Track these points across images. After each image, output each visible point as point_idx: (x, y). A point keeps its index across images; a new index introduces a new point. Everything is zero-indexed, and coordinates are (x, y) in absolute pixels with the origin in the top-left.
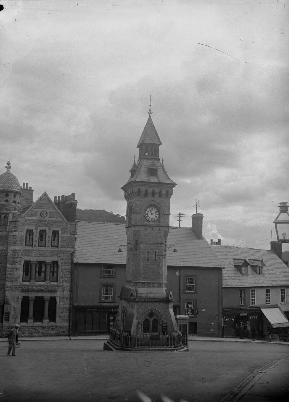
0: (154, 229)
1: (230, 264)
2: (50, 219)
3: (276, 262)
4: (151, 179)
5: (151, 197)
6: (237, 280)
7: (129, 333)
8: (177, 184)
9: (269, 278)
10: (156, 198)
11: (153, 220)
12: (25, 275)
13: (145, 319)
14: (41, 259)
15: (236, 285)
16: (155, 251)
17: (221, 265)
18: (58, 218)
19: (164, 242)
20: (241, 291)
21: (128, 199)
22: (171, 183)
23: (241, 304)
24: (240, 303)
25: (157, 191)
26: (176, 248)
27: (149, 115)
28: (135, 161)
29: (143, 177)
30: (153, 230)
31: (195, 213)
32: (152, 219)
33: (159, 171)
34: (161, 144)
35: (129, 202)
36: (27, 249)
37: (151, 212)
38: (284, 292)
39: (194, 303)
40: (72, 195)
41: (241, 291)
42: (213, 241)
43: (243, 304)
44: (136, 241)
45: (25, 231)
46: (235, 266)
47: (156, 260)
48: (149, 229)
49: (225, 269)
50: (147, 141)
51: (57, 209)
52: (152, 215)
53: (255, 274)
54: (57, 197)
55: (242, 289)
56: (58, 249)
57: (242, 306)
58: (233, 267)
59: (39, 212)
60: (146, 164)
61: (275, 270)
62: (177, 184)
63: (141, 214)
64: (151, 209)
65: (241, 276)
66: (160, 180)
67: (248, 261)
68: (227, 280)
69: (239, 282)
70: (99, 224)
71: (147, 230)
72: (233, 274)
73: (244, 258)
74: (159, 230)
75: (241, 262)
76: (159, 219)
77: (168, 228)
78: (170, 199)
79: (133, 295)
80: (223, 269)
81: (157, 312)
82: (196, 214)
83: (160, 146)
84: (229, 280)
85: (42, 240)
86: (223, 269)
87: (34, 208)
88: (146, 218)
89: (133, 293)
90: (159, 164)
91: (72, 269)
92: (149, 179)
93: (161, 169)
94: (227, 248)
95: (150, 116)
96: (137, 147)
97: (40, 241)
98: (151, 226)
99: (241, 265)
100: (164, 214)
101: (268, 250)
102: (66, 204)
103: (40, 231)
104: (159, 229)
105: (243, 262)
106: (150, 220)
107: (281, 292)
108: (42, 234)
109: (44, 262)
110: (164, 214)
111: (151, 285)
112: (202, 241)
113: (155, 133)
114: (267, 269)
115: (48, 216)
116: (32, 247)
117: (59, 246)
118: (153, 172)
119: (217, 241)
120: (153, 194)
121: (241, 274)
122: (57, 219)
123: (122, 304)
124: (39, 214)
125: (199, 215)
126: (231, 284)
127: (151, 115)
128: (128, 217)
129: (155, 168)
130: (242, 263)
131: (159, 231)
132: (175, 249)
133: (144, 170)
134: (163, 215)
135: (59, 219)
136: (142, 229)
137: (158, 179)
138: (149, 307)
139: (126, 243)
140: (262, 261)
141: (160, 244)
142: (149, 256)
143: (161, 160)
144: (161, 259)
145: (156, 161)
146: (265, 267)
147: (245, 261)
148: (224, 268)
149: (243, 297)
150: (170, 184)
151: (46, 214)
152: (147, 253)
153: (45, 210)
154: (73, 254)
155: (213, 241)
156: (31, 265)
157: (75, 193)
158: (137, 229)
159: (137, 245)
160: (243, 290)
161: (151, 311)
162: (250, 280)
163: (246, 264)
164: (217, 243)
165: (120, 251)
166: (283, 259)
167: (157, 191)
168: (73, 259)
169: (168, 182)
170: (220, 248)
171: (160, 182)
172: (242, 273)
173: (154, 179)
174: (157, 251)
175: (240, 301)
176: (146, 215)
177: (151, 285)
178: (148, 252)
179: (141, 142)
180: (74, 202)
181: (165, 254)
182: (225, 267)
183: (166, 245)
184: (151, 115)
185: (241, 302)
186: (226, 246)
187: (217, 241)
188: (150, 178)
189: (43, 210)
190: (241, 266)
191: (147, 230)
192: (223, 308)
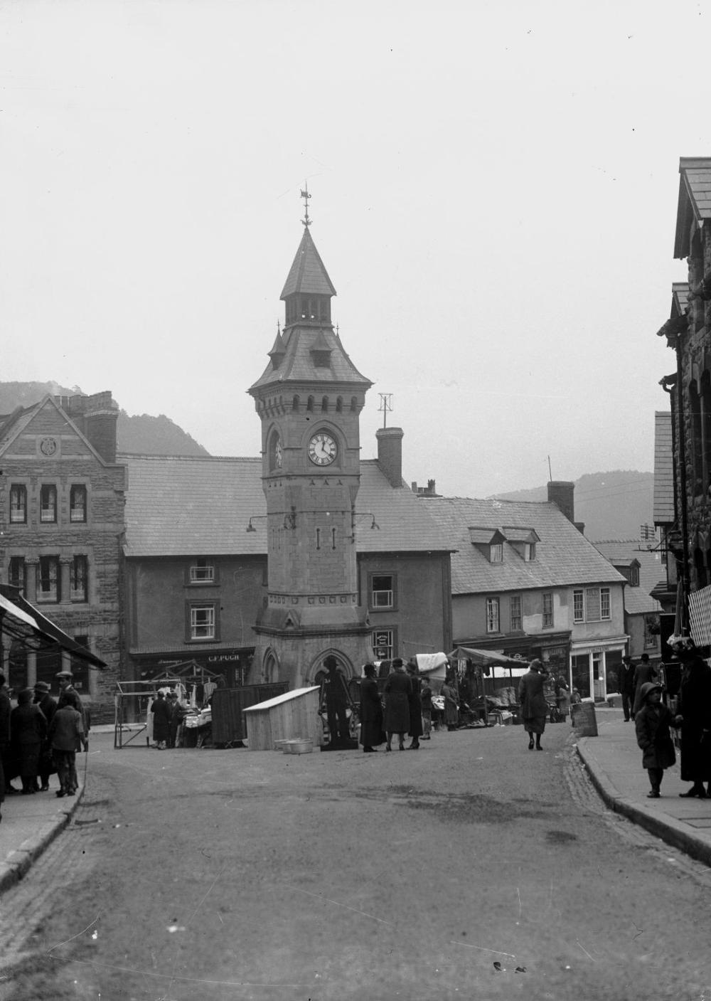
0: (329, 482)
1: (464, 541)
2: (65, 458)
3: (561, 529)
4: (318, 374)
5: (319, 412)
6: (480, 577)
7: (93, 716)
8: (373, 384)
9: (549, 567)
10: (332, 415)
11: (326, 461)
12: (198, 611)
13: (319, 670)
14: (48, 551)
15: (480, 589)
16: (332, 528)
17: (447, 545)
18: (81, 455)
19: (350, 509)
20: (490, 602)
21: (265, 416)
22: (362, 380)
23: (492, 629)
24: (489, 626)
25: (333, 399)
26: (375, 521)
27: (304, 227)
28: (279, 331)
29: (303, 370)
30: (328, 484)
31: (383, 427)
32: (322, 459)
33: (333, 354)
34: (335, 293)
35: (270, 423)
36: (14, 529)
37: (324, 444)
38: (581, 596)
39: (390, 633)
40: (103, 396)
41: (490, 602)
42: (418, 486)
43: (494, 630)
44: (293, 508)
45: (8, 487)
46: (474, 544)
47: (334, 548)
48: (319, 483)
49: (457, 553)
50: (305, 289)
51: (79, 432)
52: (321, 450)
53: (518, 560)
54: (61, 398)
55: (491, 596)
56: (87, 526)
57: (494, 633)
58: (471, 546)
59: (38, 443)
60: (305, 340)
61: (560, 548)
62: (373, 384)
63: (301, 451)
64: (325, 438)
65: (488, 566)
66: (338, 375)
67: (501, 531)
68: (460, 579)
69: (485, 580)
70: (166, 462)
71: (314, 484)
72: (471, 562)
73: (492, 526)
74: (338, 484)
75: (487, 534)
76: (336, 459)
77: (356, 477)
78: (360, 416)
79: (293, 621)
80: (451, 554)
81: (341, 655)
82: (385, 429)
83: (332, 298)
84: (464, 578)
85: (46, 507)
86: (451, 554)
87: (26, 434)
88: (311, 461)
89: (292, 619)
90: (332, 338)
91: (120, 571)
92: (316, 376)
93: (338, 351)
94: (453, 504)
95: (307, 230)
96: (281, 299)
97: (42, 510)
98: (324, 475)
99: (488, 542)
100: (349, 449)
101: (543, 503)
102: (86, 416)
103: (43, 485)
104: (340, 481)
105: (492, 534)
106: (320, 461)
107: (575, 596)
108: (48, 490)
109: (55, 558)
110: (349, 449)
111: (327, 601)
112: (402, 490)
113: (320, 270)
114: (543, 546)
115: (59, 451)
116: (25, 525)
117: (89, 520)
118: (321, 357)
119: (427, 486)
120: (325, 406)
121: (490, 561)
122: (80, 458)
123: (263, 644)
124: (38, 447)
125: (392, 432)
126: (469, 585)
127: (309, 227)
128: (267, 455)
129: (327, 349)
130: (491, 538)
131: (340, 486)
132: (373, 523)
133: (304, 354)
134: (348, 451)
135: (86, 457)
136: (305, 483)
137: (334, 374)
138: (326, 643)
139: (266, 512)
140: (533, 530)
141: (343, 512)
142: (321, 540)
143: (334, 330)
144: (345, 545)
145: (325, 333)
146: (538, 543)
147: (497, 531)
148: (454, 552)
149: (494, 613)
150: (359, 383)
151: (53, 447)
152: (316, 533)
153: (51, 436)
154: (121, 536)
155: (418, 486)
156: (25, 566)
157: (110, 392)
158: (294, 482)
159: (294, 516)
160: (493, 598)
161: (330, 654)
162: (508, 574)
163: (499, 538)
164: (425, 489)
165: (250, 529)
166: (575, 521)
167: (333, 399)
168: (122, 547)
169: (355, 379)
170: (439, 504)
171: (339, 380)
172: (492, 560)
173: (324, 375)
174: (337, 528)
175: (489, 623)
176: (312, 452)
177: (327, 601)
178: (318, 530)
179: (293, 291)
180: (109, 414)
181: (353, 535)
182: (455, 548)
183: (353, 514)
184: (309, 227)
185: (492, 625)
186: (452, 499)
187: (427, 486)
188: (316, 370)
189: (47, 436)
190: (489, 545)
191: (314, 484)
192: (455, 641)
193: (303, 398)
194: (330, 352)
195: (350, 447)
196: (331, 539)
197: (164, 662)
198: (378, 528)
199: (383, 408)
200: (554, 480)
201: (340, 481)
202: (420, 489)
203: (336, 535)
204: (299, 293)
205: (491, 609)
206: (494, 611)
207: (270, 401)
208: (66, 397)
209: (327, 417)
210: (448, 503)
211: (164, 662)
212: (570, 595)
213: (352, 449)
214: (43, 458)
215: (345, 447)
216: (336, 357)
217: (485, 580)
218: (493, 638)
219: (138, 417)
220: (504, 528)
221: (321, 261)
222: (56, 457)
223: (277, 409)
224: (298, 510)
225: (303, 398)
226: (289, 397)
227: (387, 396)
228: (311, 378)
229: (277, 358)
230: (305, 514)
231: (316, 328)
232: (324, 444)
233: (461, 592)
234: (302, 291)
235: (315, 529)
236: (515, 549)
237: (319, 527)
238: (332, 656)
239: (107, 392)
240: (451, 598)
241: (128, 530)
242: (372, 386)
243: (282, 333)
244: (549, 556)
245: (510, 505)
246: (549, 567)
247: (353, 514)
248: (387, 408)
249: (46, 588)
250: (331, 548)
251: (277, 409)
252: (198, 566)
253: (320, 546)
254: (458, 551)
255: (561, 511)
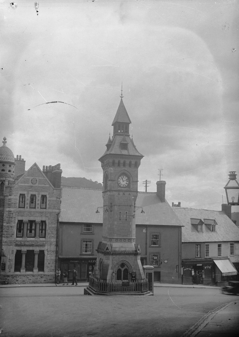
2: (40, 185)
8: (144, 156)
9: (221, 234)
10: (127, 168)
13: (119, 268)
14: (32, 219)
19: (133, 205)
20: (197, 245)
22: (139, 155)
25: (128, 162)
26: (143, 210)
29: (116, 150)
31: (159, 180)
34: (131, 123)
38: (233, 246)
39: (158, 255)
41: (197, 245)
42: (174, 204)
44: (111, 204)
47: (126, 220)
49: (184, 227)
52: (123, 182)
57: (198, 258)
59: (30, 180)
60: (119, 139)
67: (203, 220)
68: (186, 236)
73: (200, 218)
75: (197, 221)
80: (182, 227)
82: (160, 181)
84: (187, 237)
88: (119, 185)
89: (108, 247)
95: (122, 99)
96: (112, 125)
99: (197, 224)
104: (129, 194)
105: (199, 221)
108: (33, 198)
110: (133, 181)
118: (124, 146)
119: (178, 204)
121: (198, 231)
122: (45, 186)
131: (129, 196)
132: (142, 211)
134: (133, 182)
135: (47, 185)
136: (116, 193)
137: (128, 152)
138: (121, 258)
139: (103, 206)
140: (215, 220)
141: (130, 206)
142: (121, 216)
145: (126, 137)
146: (217, 225)
147: (201, 220)
148: (183, 226)
150: (138, 156)
151: (36, 181)
155: (174, 204)
157: (60, 164)
158: (112, 193)
162: (204, 236)
163: (201, 223)
167: (128, 162)
169: (137, 154)
171: (130, 154)
173: (125, 152)
174: (127, 212)
176: (119, 182)
179: (115, 121)
183: (135, 207)
187: (178, 204)
188: (121, 151)
190: (197, 225)
193: (117, 161)
194: (128, 144)
195: (134, 181)
196: (125, 216)
197: (72, 261)
198: (144, 213)
199: (160, 174)
200: (224, 203)
201: (129, 194)
202: (175, 205)
203: (127, 215)
204: (117, 122)
205: (197, 248)
206: (199, 249)
207: (105, 162)
208: (47, 166)
209: (126, 169)
210: (183, 209)
211: (72, 261)
212: (229, 245)
213: (134, 181)
214: (32, 185)
215: (132, 181)
216: (130, 146)
217: (196, 238)
218: (198, 260)
219: (81, 178)
220: (204, 219)
221: (126, 111)
222: (37, 185)
223: (107, 165)
224: (113, 204)
225: (117, 161)
226: (111, 161)
227: (161, 170)
228: (119, 153)
229: (109, 146)
230: (116, 206)
231: (122, 135)
232: (122, 179)
233: (186, 242)
234: (118, 121)
235: (125, 212)
236: (208, 227)
237: (121, 212)
238: (123, 263)
239: (59, 164)
240: (181, 244)
241: (61, 212)
242: (143, 157)
243: (111, 138)
244: (221, 230)
245: (207, 211)
246: (221, 234)
247: (135, 207)
248: (161, 174)
249: (31, 232)
250: (125, 220)
251: (107, 165)
252: (87, 227)
253: (127, 219)
254: (184, 226)
255: (226, 214)
